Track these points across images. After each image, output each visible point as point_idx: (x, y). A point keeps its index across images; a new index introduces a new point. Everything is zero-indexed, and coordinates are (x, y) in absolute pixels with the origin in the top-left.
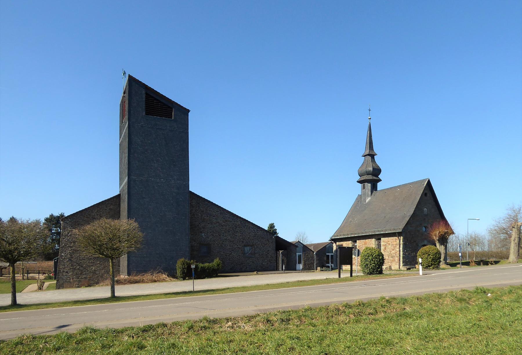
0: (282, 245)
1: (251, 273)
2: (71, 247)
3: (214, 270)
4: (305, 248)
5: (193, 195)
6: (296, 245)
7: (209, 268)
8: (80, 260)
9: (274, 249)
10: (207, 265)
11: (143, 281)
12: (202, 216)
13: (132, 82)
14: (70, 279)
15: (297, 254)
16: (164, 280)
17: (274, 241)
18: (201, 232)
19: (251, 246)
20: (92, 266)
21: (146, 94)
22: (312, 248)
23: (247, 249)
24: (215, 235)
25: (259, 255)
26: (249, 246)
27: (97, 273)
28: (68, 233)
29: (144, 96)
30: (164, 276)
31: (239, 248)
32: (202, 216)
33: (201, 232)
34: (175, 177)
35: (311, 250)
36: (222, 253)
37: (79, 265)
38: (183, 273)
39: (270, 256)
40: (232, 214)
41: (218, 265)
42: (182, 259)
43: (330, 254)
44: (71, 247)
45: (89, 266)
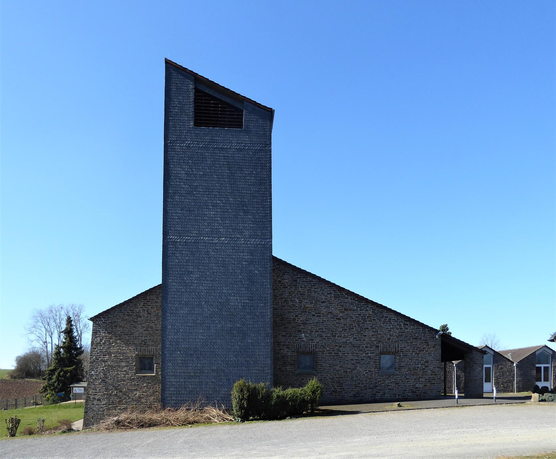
0: (451, 348)
1: (387, 406)
2: (104, 361)
3: (303, 401)
4: (498, 357)
5: (281, 265)
6: (483, 350)
7: (293, 399)
8: (118, 381)
9: (439, 357)
10: (290, 391)
11: (166, 423)
12: (301, 302)
13: (171, 68)
14: (104, 411)
15: (485, 366)
16: (208, 421)
17: (439, 343)
18: (300, 331)
19: (394, 353)
20: (136, 390)
21: (197, 90)
22: (509, 356)
23: (386, 361)
24: (324, 335)
25: (409, 369)
26: (389, 353)
27: (143, 400)
28: (101, 340)
29: (192, 95)
30: (215, 412)
31: (370, 357)
32: (301, 302)
33: (300, 331)
34: (247, 233)
35: (509, 360)
36: (338, 368)
37: (117, 389)
38: (241, 407)
39: (429, 372)
40: (357, 296)
41: (314, 392)
42: (241, 382)
43: (542, 366)
44: (104, 361)
45: (132, 391)
